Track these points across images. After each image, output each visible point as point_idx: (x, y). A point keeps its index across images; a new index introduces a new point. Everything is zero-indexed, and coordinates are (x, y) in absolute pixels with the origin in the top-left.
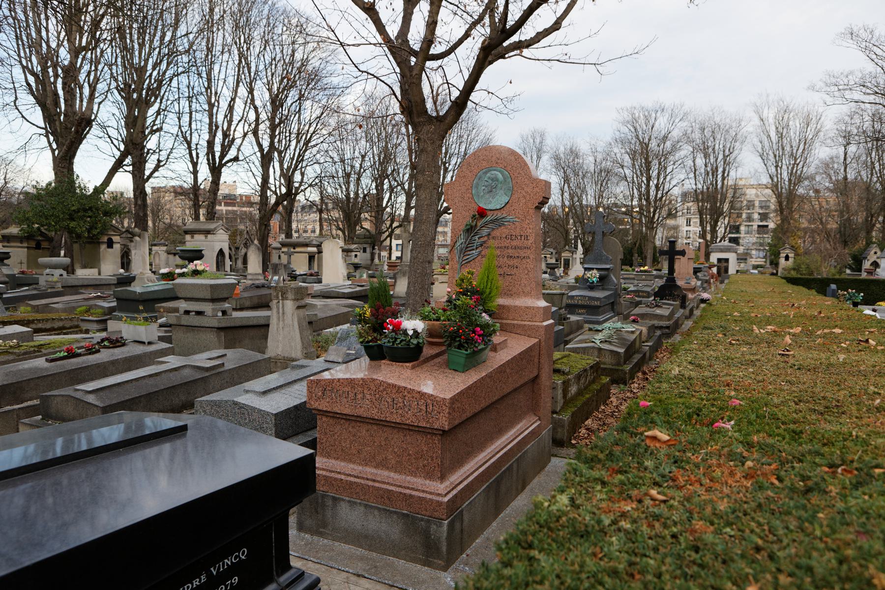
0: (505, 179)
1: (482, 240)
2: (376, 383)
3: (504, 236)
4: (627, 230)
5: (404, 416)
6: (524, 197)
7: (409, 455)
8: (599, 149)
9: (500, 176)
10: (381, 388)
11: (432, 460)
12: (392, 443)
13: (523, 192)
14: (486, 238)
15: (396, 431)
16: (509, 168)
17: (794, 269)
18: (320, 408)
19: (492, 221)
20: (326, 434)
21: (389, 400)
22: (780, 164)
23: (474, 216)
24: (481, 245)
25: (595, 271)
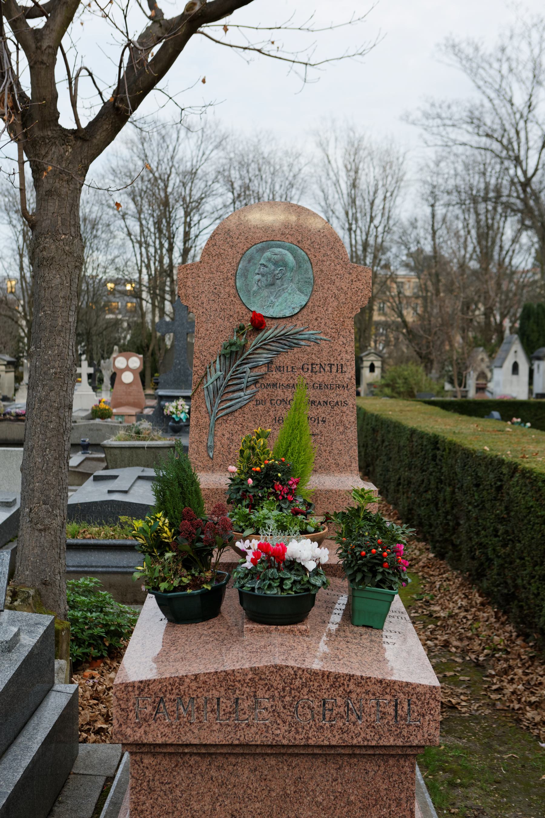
1: (257, 372)
2: (285, 673)
3: (300, 365)
4: (117, 323)
5: (348, 732)
6: (336, 297)
7: (349, 803)
9: (290, 258)
10: (298, 683)
11: (399, 805)
12: (312, 785)
13: (333, 288)
14: (264, 370)
15: (318, 762)
16: (306, 244)
17: (388, 385)
18: (150, 739)
19: (277, 339)
20: (151, 790)
21: (315, 704)
22: (354, 227)
23: (242, 328)
24: (256, 382)
25: (181, 402)
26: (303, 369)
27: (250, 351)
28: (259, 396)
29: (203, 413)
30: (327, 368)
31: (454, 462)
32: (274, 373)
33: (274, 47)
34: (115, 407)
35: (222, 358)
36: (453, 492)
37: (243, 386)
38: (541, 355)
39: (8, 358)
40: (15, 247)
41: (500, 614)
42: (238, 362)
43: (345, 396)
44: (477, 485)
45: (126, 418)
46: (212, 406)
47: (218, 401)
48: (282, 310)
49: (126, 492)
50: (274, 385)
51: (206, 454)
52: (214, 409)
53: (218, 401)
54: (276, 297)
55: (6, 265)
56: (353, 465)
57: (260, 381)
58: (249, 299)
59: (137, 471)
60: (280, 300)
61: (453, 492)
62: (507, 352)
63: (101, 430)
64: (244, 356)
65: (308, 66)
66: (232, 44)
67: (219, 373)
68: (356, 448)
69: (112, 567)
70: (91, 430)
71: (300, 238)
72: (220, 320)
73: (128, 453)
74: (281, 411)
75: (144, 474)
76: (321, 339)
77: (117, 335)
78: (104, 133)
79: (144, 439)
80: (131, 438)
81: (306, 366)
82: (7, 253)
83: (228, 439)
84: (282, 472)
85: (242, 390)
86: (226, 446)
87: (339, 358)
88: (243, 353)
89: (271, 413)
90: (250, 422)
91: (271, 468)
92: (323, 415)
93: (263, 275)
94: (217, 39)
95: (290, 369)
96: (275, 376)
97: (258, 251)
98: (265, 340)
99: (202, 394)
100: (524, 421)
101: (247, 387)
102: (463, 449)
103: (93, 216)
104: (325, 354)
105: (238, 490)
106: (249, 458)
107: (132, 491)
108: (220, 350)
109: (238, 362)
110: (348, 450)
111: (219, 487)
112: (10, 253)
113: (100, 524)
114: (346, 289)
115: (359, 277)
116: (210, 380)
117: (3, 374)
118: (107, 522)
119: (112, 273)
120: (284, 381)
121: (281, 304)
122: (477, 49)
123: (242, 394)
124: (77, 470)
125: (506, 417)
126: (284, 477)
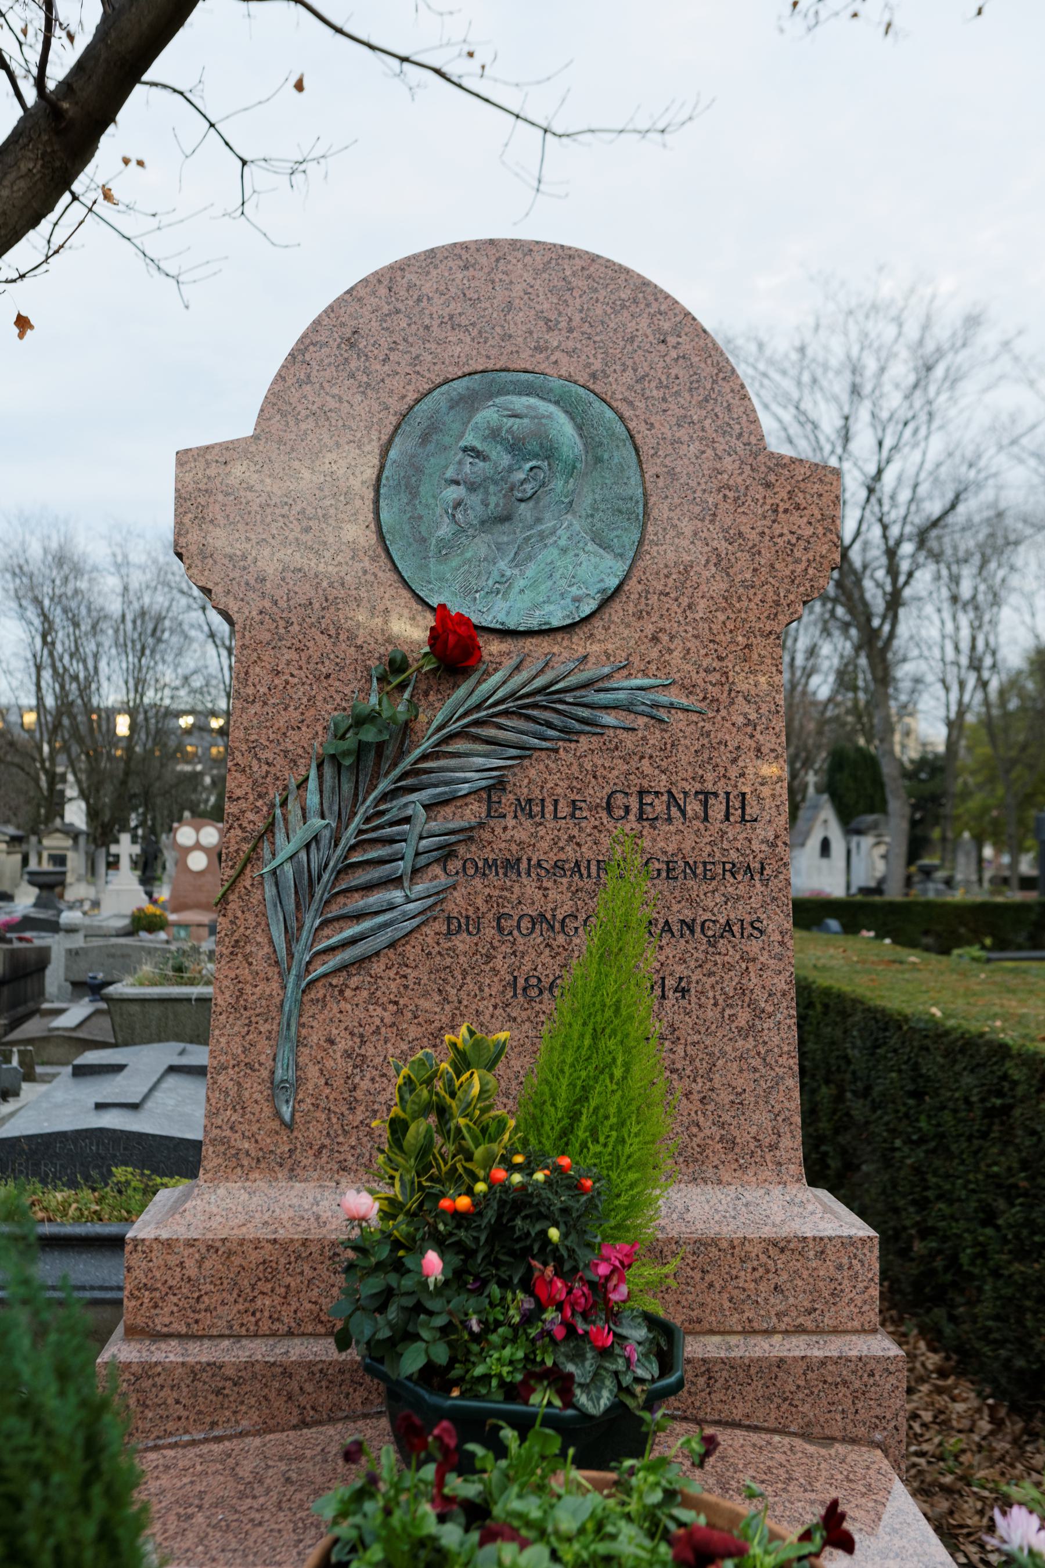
0: (592, 444)
3: (597, 794)
4: (196, 776)
8: (133, 558)
9: (563, 428)
14: (473, 812)
19: (522, 705)
24: (446, 854)
26: (609, 808)
27: (425, 746)
28: (457, 903)
29: (260, 965)
30: (693, 807)
31: (839, 1033)
32: (510, 822)
33: (474, 65)
34: (175, 910)
35: (328, 770)
36: (839, 1098)
37: (401, 867)
38: (863, 826)
39: (11, 830)
40: (30, 656)
41: (1002, 1413)
42: (384, 785)
43: (755, 902)
44: (918, 1095)
45: (193, 929)
46: (291, 938)
47: (311, 921)
48: (536, 606)
49: (135, 1107)
50: (511, 865)
51: (267, 1111)
52: (298, 948)
53: (311, 921)
54: (517, 562)
55: (15, 683)
56: (786, 1142)
57: (461, 850)
58: (423, 567)
59: (166, 1053)
60: (531, 570)
61: (839, 1098)
62: (812, 819)
63: (129, 956)
64: (405, 764)
65: (549, 136)
66: (374, 42)
67: (316, 822)
68: (792, 1083)
69: (92, 1288)
70: (113, 956)
71: (597, 365)
72: (322, 639)
73: (157, 1011)
74: (535, 957)
75: (184, 1061)
76: (672, 706)
77: (193, 797)
78: (22, 184)
79: (191, 982)
80: (165, 980)
81: (620, 800)
82: (18, 664)
83: (348, 1055)
84: (566, 1218)
85: (396, 881)
86: (338, 1082)
87: (733, 772)
88: (401, 754)
89: (498, 962)
90: (426, 994)
91: (516, 1204)
92: (680, 970)
93: (472, 488)
94: (338, 23)
95: (564, 810)
96: (513, 832)
97: (453, 404)
98: (478, 707)
99: (256, 896)
100: (880, 936)
101: (415, 871)
102: (869, 1010)
103: (156, 607)
104: (684, 757)
105: (385, 1298)
106: (425, 1150)
107: (149, 1104)
108: (321, 743)
109: (384, 785)
110: (768, 1092)
111: (315, 1234)
112: (21, 664)
113: (72, 1184)
114: (753, 536)
115: (800, 498)
116: (286, 848)
117: (4, 856)
118: (87, 1178)
119: (185, 699)
120: (543, 851)
121: (534, 584)
122: (761, 346)
123: (397, 895)
124: (80, 1034)
125: (851, 928)
126: (572, 1240)
